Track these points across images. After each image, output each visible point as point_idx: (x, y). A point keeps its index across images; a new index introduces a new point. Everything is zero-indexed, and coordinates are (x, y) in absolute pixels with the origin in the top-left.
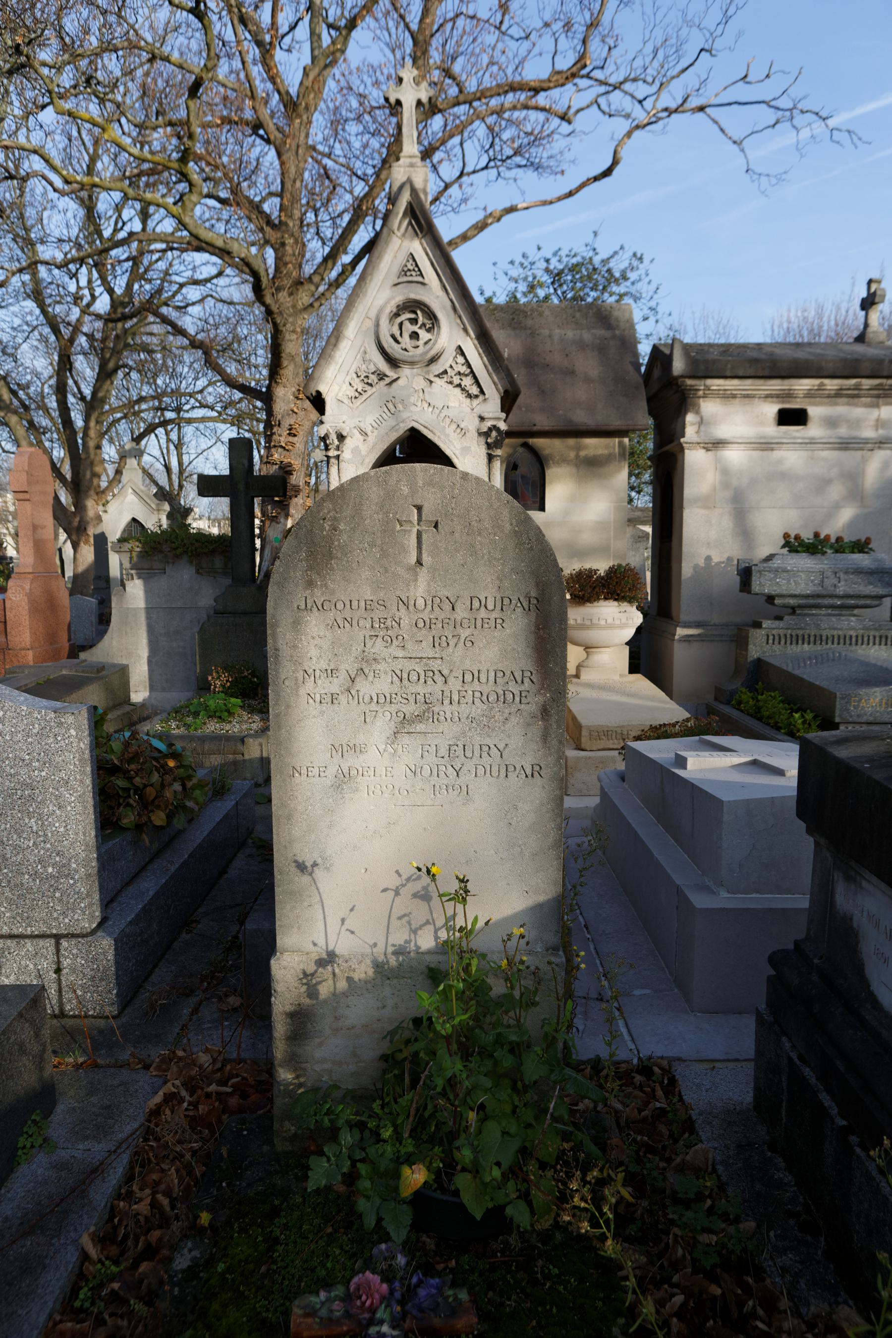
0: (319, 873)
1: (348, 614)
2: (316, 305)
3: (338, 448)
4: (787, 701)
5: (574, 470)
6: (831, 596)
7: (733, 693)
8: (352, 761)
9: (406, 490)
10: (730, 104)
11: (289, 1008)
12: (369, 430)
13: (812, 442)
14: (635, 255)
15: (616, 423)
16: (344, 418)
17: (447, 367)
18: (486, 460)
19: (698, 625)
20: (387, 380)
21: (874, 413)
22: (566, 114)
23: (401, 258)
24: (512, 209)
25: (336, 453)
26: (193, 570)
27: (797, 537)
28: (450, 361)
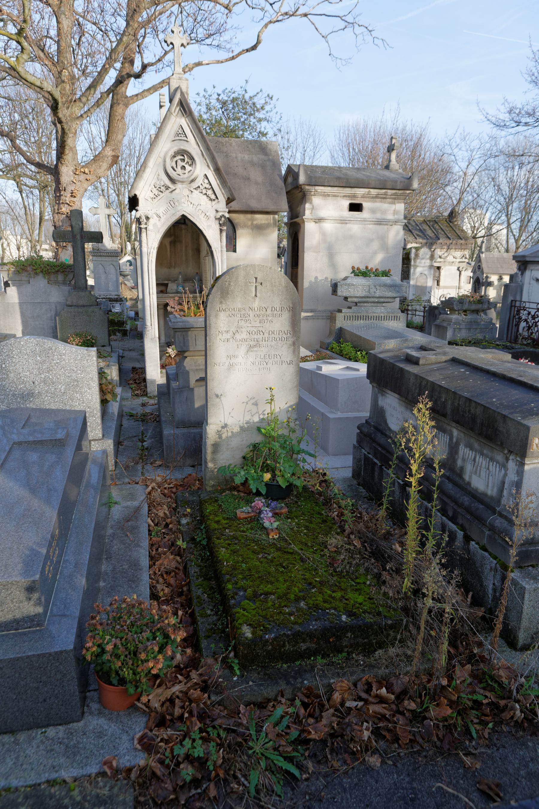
0: (222, 398)
1: (233, 312)
2: (85, 116)
3: (146, 224)
4: (354, 347)
5: (250, 231)
6: (373, 297)
7: (329, 344)
8: (233, 360)
9: (252, 272)
10: (321, 15)
11: (212, 443)
12: (161, 215)
13: (365, 220)
14: (268, 95)
15: (271, 208)
16: (149, 208)
17: (200, 184)
18: (219, 232)
19: (312, 311)
20: (170, 190)
21: (393, 207)
22: (228, 5)
23: (176, 128)
24: (199, 64)
25: (145, 226)
26: (46, 281)
27: (358, 269)
28: (201, 182)
